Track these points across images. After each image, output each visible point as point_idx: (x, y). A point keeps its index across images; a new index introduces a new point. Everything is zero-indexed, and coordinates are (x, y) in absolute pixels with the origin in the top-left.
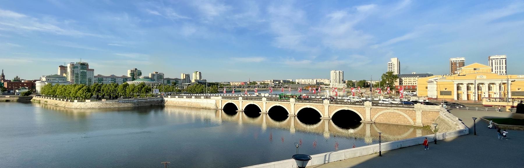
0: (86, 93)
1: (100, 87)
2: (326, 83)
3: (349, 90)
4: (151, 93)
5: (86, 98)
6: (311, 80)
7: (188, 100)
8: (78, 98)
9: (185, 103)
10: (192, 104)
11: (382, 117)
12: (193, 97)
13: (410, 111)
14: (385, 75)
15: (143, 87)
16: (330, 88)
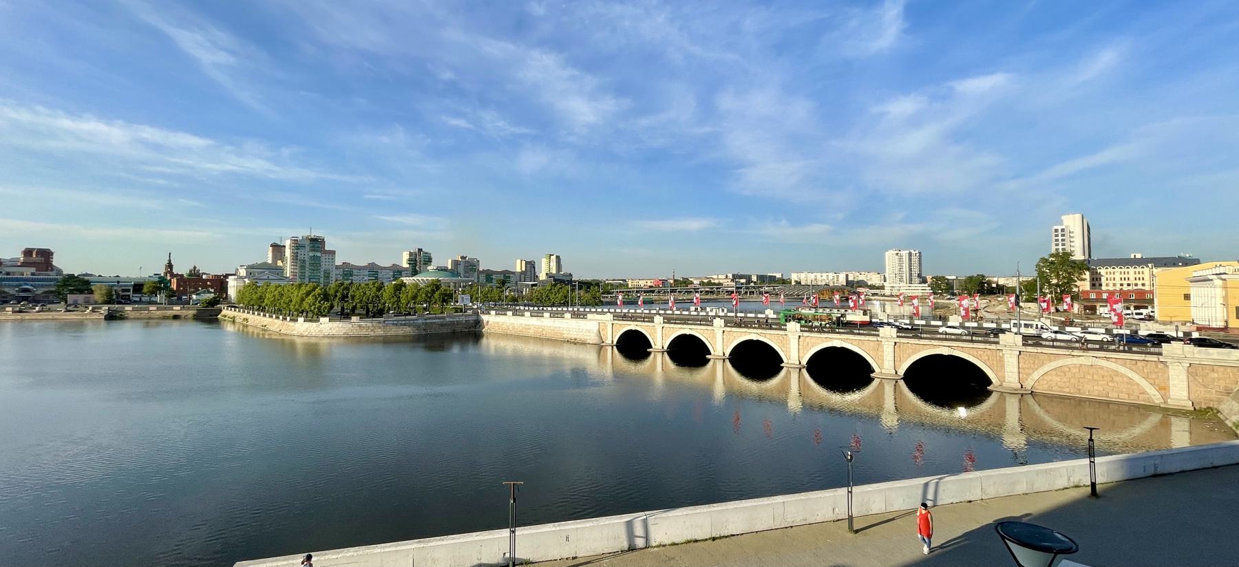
0: (320, 302)
1: (347, 289)
2: (874, 283)
3: (939, 301)
4: (452, 304)
5: (320, 314)
6: (831, 275)
7: (535, 321)
8: (305, 314)
9: (528, 327)
10: (543, 330)
11: (1058, 379)
12: (547, 315)
13: (1149, 363)
14: (1047, 260)
15: (437, 291)
16: (884, 295)
